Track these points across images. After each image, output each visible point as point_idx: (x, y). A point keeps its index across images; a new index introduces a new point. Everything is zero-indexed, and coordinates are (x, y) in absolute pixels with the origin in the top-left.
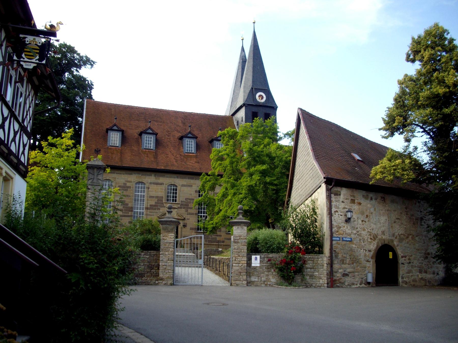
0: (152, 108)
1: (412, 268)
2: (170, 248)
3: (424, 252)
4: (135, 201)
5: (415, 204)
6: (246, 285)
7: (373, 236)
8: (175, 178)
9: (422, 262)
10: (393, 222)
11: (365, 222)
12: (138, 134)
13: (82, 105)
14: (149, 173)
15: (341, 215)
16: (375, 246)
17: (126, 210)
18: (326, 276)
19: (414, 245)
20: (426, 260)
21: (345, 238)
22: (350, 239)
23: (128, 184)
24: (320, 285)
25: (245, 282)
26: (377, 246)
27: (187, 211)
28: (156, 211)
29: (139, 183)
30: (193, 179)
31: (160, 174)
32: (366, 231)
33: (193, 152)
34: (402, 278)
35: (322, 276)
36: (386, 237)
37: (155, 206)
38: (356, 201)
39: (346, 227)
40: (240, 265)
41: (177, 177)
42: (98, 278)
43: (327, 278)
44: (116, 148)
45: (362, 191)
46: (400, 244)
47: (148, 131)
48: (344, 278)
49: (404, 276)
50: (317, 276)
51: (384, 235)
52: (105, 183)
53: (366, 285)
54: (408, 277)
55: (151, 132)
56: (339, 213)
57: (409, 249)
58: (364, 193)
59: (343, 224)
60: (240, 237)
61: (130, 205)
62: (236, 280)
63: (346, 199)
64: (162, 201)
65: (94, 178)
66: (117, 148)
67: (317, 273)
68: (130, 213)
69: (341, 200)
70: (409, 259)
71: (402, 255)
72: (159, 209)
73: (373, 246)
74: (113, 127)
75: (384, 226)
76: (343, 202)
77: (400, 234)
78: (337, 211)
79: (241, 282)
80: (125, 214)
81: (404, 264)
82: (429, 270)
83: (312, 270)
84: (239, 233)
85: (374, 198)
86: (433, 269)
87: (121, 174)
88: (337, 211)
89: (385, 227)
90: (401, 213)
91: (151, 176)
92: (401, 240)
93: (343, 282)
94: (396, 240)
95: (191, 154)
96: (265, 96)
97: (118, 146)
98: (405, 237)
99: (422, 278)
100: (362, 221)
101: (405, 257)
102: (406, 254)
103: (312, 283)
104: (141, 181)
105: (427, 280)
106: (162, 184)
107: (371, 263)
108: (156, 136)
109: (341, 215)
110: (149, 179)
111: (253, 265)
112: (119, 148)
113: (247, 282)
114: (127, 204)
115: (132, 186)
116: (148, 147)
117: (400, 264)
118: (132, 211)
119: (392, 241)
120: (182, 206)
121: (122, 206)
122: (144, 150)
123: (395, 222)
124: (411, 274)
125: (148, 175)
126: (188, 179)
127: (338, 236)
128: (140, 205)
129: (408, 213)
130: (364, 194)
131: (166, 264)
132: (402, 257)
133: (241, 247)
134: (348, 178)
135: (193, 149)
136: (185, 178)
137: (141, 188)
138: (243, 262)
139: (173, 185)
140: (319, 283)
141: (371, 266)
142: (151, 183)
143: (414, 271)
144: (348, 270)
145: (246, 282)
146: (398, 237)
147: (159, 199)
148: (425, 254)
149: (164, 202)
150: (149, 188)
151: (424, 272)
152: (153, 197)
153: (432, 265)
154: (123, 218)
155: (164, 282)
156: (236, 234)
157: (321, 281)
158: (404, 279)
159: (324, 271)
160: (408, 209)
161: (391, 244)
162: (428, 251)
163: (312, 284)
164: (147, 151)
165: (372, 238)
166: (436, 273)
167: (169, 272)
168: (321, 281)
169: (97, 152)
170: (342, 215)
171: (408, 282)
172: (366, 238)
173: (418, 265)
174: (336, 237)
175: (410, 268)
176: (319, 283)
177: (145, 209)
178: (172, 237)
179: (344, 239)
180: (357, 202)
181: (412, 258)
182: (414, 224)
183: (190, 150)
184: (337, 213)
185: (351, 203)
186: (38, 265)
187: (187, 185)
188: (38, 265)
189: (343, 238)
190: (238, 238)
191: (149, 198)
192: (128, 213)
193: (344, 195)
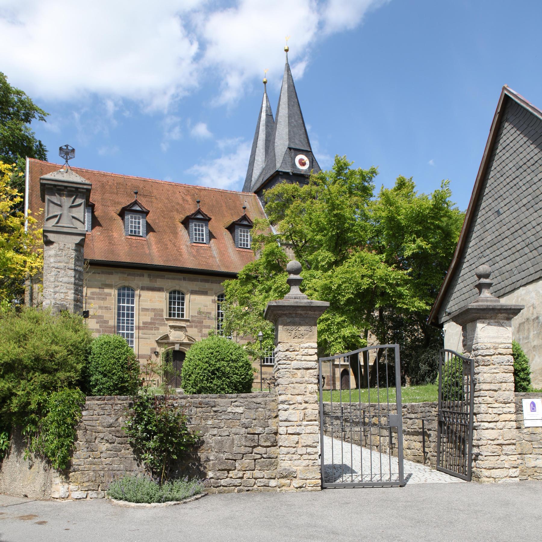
8: (180, 279)
12: (118, 213)
14: (139, 272)
25: (514, 470)
27: (201, 331)
28: (153, 332)
29: (124, 288)
30: (207, 281)
33: (205, 242)
37: (151, 323)
40: (500, 425)
41: (184, 279)
47: (134, 208)
55: (138, 208)
65: (61, 215)
72: (158, 329)
79: (504, 472)
84: (493, 338)
91: (143, 276)
96: (308, 162)
111: (527, 424)
114: (107, 322)
120: (193, 324)
121: (98, 325)
126: (201, 282)
131: (298, 430)
135: (204, 237)
136: (196, 280)
137: (179, 299)
138: (508, 417)
147: (157, 312)
149: (165, 317)
150: (140, 296)
152: (147, 310)
155: (296, 483)
156: (486, 340)
164: (134, 238)
167: (309, 454)
169: (67, 153)
183: (199, 239)
190: (492, 351)
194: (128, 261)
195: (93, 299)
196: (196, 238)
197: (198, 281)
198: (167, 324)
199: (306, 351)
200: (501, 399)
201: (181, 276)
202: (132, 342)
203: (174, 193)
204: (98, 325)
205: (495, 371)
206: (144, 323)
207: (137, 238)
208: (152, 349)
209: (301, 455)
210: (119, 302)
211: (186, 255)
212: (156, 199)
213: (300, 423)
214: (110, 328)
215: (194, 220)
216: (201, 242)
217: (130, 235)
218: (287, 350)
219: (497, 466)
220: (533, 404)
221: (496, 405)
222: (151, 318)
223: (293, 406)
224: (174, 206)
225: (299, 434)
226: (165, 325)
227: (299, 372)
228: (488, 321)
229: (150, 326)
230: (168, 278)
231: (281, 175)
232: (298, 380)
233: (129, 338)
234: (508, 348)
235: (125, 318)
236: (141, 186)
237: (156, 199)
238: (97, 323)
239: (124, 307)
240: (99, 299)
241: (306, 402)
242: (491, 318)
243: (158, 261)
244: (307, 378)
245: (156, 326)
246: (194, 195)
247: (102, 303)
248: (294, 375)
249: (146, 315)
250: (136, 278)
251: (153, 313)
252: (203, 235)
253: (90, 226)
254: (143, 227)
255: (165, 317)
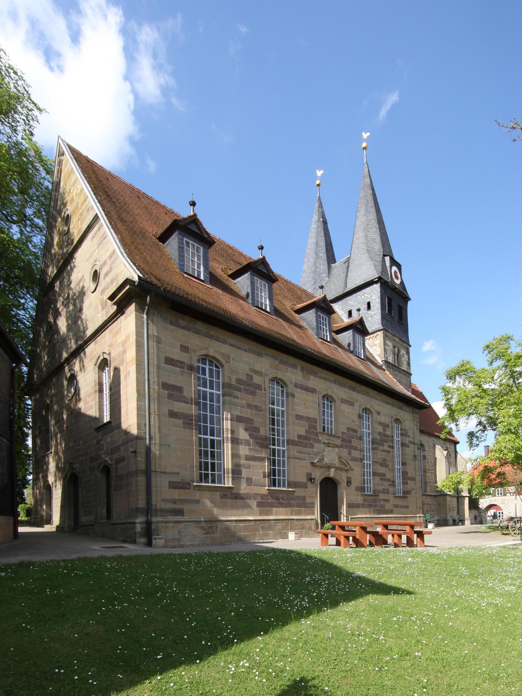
13: (103, 445)
23: (257, 379)
37: (306, 438)
42: (26, 197)
72: (312, 446)
106: (313, 391)
142: (296, 386)
149: (318, 431)
154: (252, 463)
186: (148, 297)
188: (148, 297)
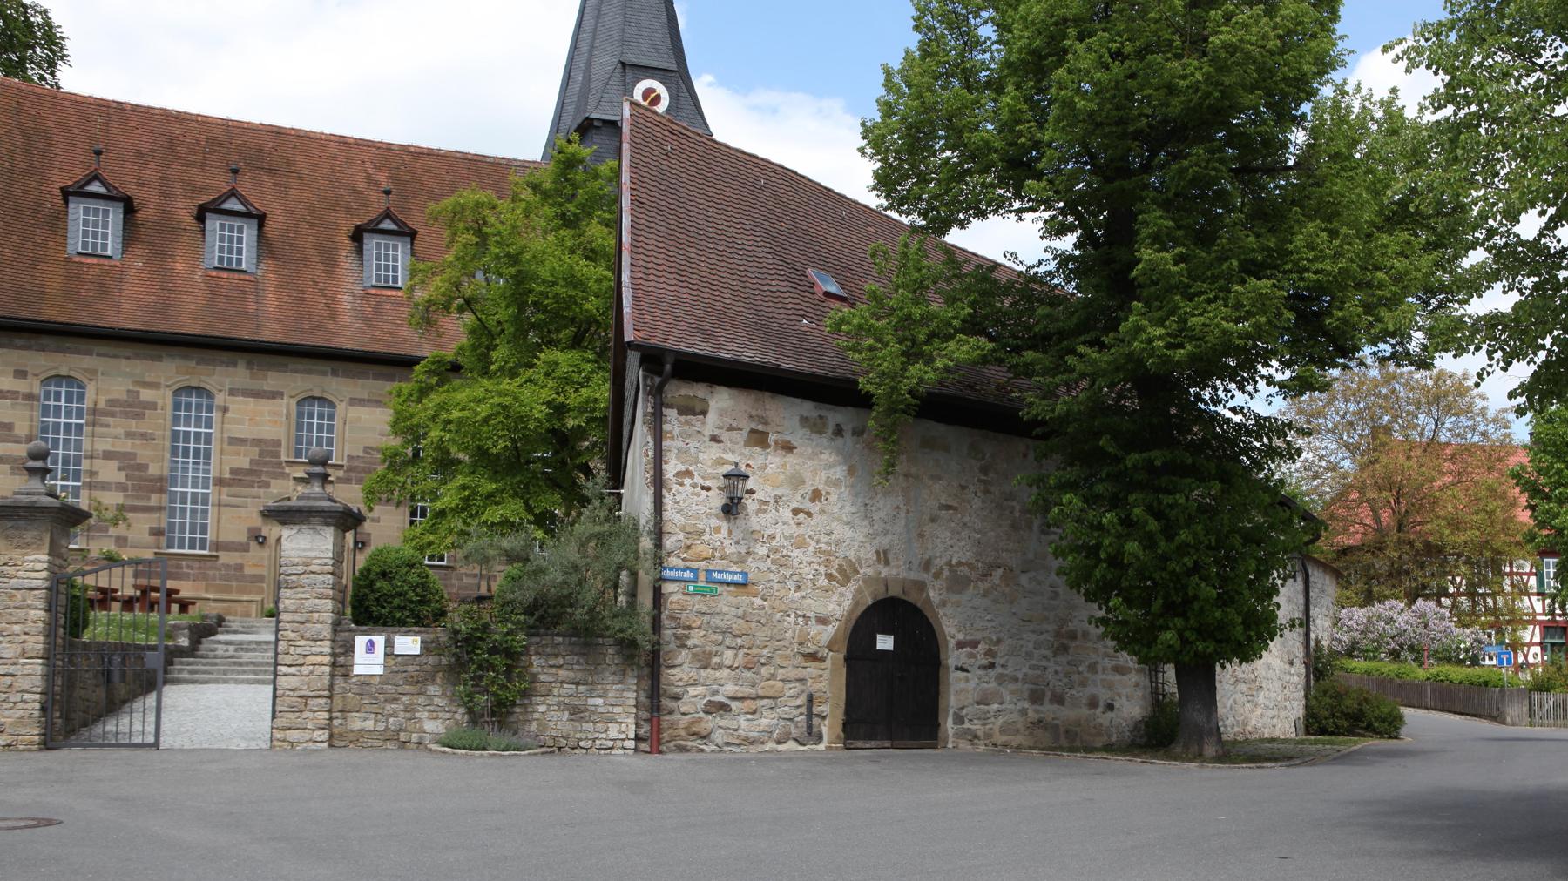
0: (257, 122)
1: (1000, 684)
2: (30, 607)
3: (1051, 627)
4: (174, 451)
5: (1025, 456)
6: (325, 745)
7: (840, 566)
8: (324, 374)
9: (1044, 663)
10: (926, 517)
11: (809, 514)
14: (225, 356)
15: (703, 488)
16: (847, 604)
17: (140, 488)
18: (634, 710)
19: (1012, 603)
20: (1062, 659)
21: (720, 572)
22: (738, 578)
24: (610, 744)
25: (321, 732)
26: (856, 604)
28: (255, 491)
29: (189, 389)
31: (268, 358)
32: (811, 549)
34: (959, 719)
35: (618, 710)
36: (896, 571)
37: (250, 472)
38: (772, 438)
39: (724, 531)
40: (305, 670)
43: (637, 718)
44: (102, 261)
45: (798, 401)
46: (955, 598)
47: (226, 206)
48: (710, 717)
49: (964, 712)
50: (600, 710)
51: (887, 563)
52: (53, 389)
53: (801, 744)
54: (984, 719)
55: (239, 207)
56: (698, 480)
57: (989, 617)
58: (807, 408)
59: (714, 522)
60: (307, 565)
61: (154, 470)
62: (290, 729)
63: (731, 429)
64: (277, 455)
66: (106, 262)
67: (599, 701)
68: (154, 500)
69: (708, 432)
70: (989, 653)
71: (960, 637)
72: (267, 485)
73: (840, 604)
74: (88, 183)
75: (886, 533)
76: (714, 439)
77: (953, 562)
78: (688, 473)
79: (306, 735)
80: (136, 503)
81: (967, 671)
82: (1074, 692)
83: (581, 688)
84: (304, 550)
85: (848, 428)
86: (1090, 690)
87: (115, 356)
88: (688, 473)
89: (890, 537)
90: (963, 488)
91: (235, 364)
92: (957, 583)
93: (704, 733)
94: (938, 584)
95: (389, 293)
97: (110, 257)
98: (974, 576)
99: (1040, 721)
100: (796, 512)
101: (974, 644)
102: (978, 636)
103: (578, 735)
104: (194, 383)
105: (1062, 730)
106: (275, 395)
107: (828, 663)
108: (261, 226)
109: (703, 488)
110: (222, 378)
111: (357, 670)
112: (112, 263)
113: (331, 736)
114: (143, 467)
115: (160, 403)
116: (230, 260)
117: (952, 669)
118: (162, 491)
119: (921, 586)
120: (353, 475)
121: (123, 474)
122: (214, 274)
123: (933, 520)
124: (995, 706)
125: (222, 363)
127: (688, 563)
128: (196, 470)
129: (992, 489)
130: (805, 414)
131: (11, 669)
132: (960, 645)
133: (307, 603)
134: (748, 353)
137: (321, 417)
138: (319, 659)
139: (319, 398)
140: (604, 736)
141: (826, 675)
143: (1007, 698)
144: (730, 689)
145: (325, 735)
146: (946, 573)
147: (267, 448)
148: (1058, 634)
149: (284, 458)
150: (225, 410)
151: (1052, 702)
152: (242, 441)
153: (1086, 674)
156: (292, 553)
157: (613, 731)
158: (967, 725)
159: (625, 694)
160: (991, 475)
161: (913, 598)
162: (1071, 626)
163: (581, 740)
164: (225, 275)
165: (835, 573)
166: (1102, 703)
167: (26, 702)
168: (613, 731)
170: (708, 489)
171: (980, 733)
172: (808, 572)
173: (1025, 675)
174: (677, 569)
175: (993, 685)
176: (604, 736)
177: (215, 485)
178: (39, 566)
179: (715, 575)
180: (776, 442)
181: (1001, 649)
182: (1014, 527)
184: (687, 481)
185: (748, 444)
187: (369, 401)
189: (708, 572)
190: (300, 569)
191: (225, 446)
192: (149, 499)
193: (722, 413)
194: (198, 331)
195: (113, 415)
196: (378, 277)
197: (368, 378)
198: (288, 475)
199: (31, 565)
200: (308, 635)
201: (326, 366)
202: (205, 512)
203: (349, 162)
204: (123, 474)
205: (303, 596)
206: (233, 471)
207: (231, 275)
208: (250, 530)
209: (15, 703)
210: (176, 420)
211: (345, 318)
212: (300, 178)
213: (14, 661)
214: (151, 481)
215: (375, 236)
216: (391, 284)
217: (216, 268)
218: (5, 564)
219: (294, 725)
220: (371, 643)
221: (302, 643)
222: (252, 460)
223: (8, 638)
224: (342, 197)
225: (13, 675)
226: (285, 476)
227: (18, 594)
228: (298, 527)
229: (249, 478)
230: (296, 372)
231: (597, 128)
232: (18, 603)
233: (196, 503)
234: (326, 564)
235: (191, 460)
236: (268, 147)
237: (300, 178)
238: (120, 469)
239: (187, 434)
240: (126, 415)
241: (26, 633)
242: (302, 522)
243: (271, 333)
244: (29, 602)
245: (263, 478)
246: (398, 169)
247: (133, 425)
248: (12, 597)
249: (238, 454)
250: (218, 369)
251: (257, 449)
252: (395, 269)
253: (120, 247)
254: (248, 251)
255: (284, 458)
